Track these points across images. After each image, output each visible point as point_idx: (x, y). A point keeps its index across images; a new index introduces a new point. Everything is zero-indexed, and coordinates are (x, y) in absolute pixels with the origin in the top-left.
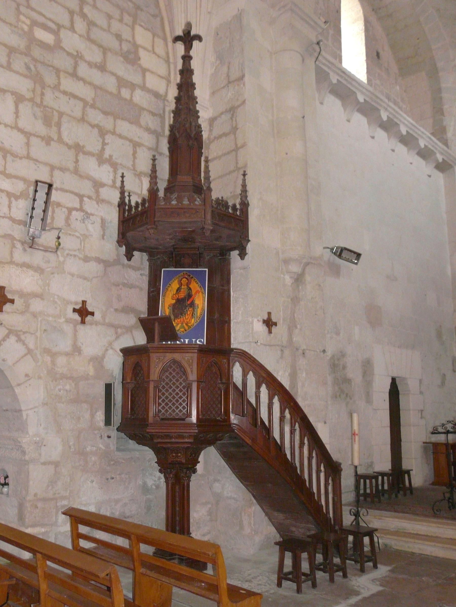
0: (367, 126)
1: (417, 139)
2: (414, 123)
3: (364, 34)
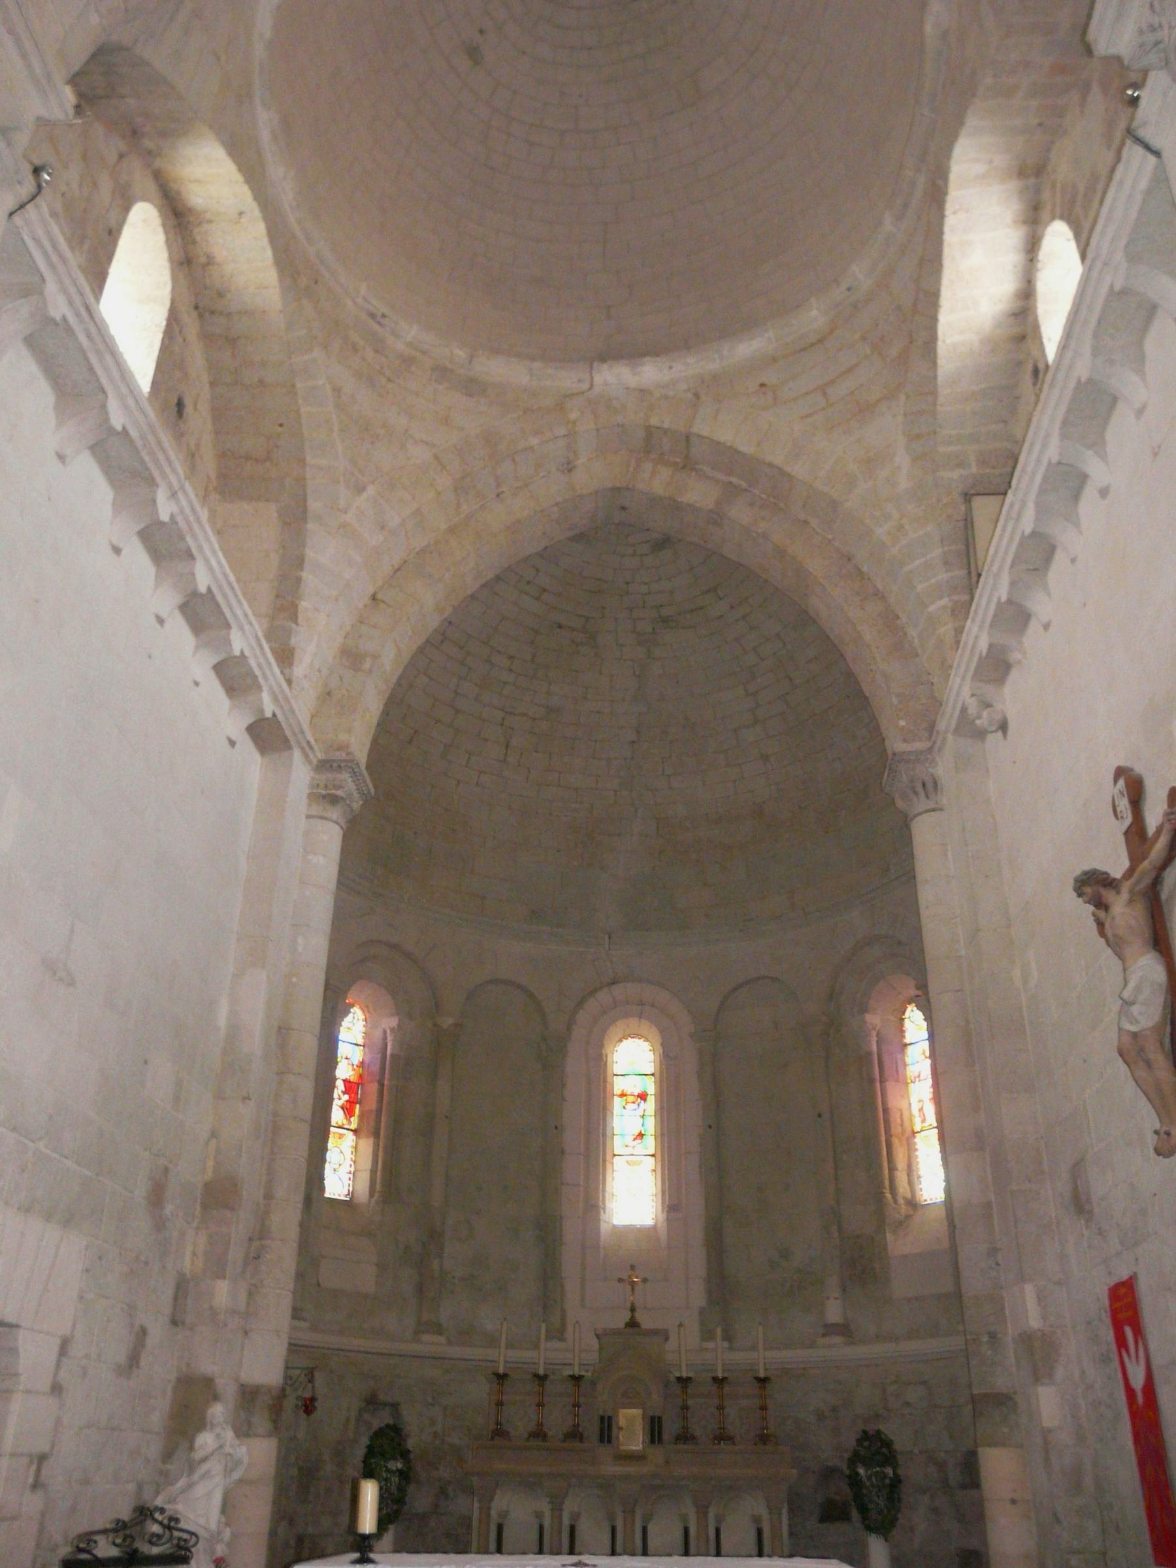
0: (108, 510)
1: (228, 626)
2: (232, 578)
3: (160, 336)
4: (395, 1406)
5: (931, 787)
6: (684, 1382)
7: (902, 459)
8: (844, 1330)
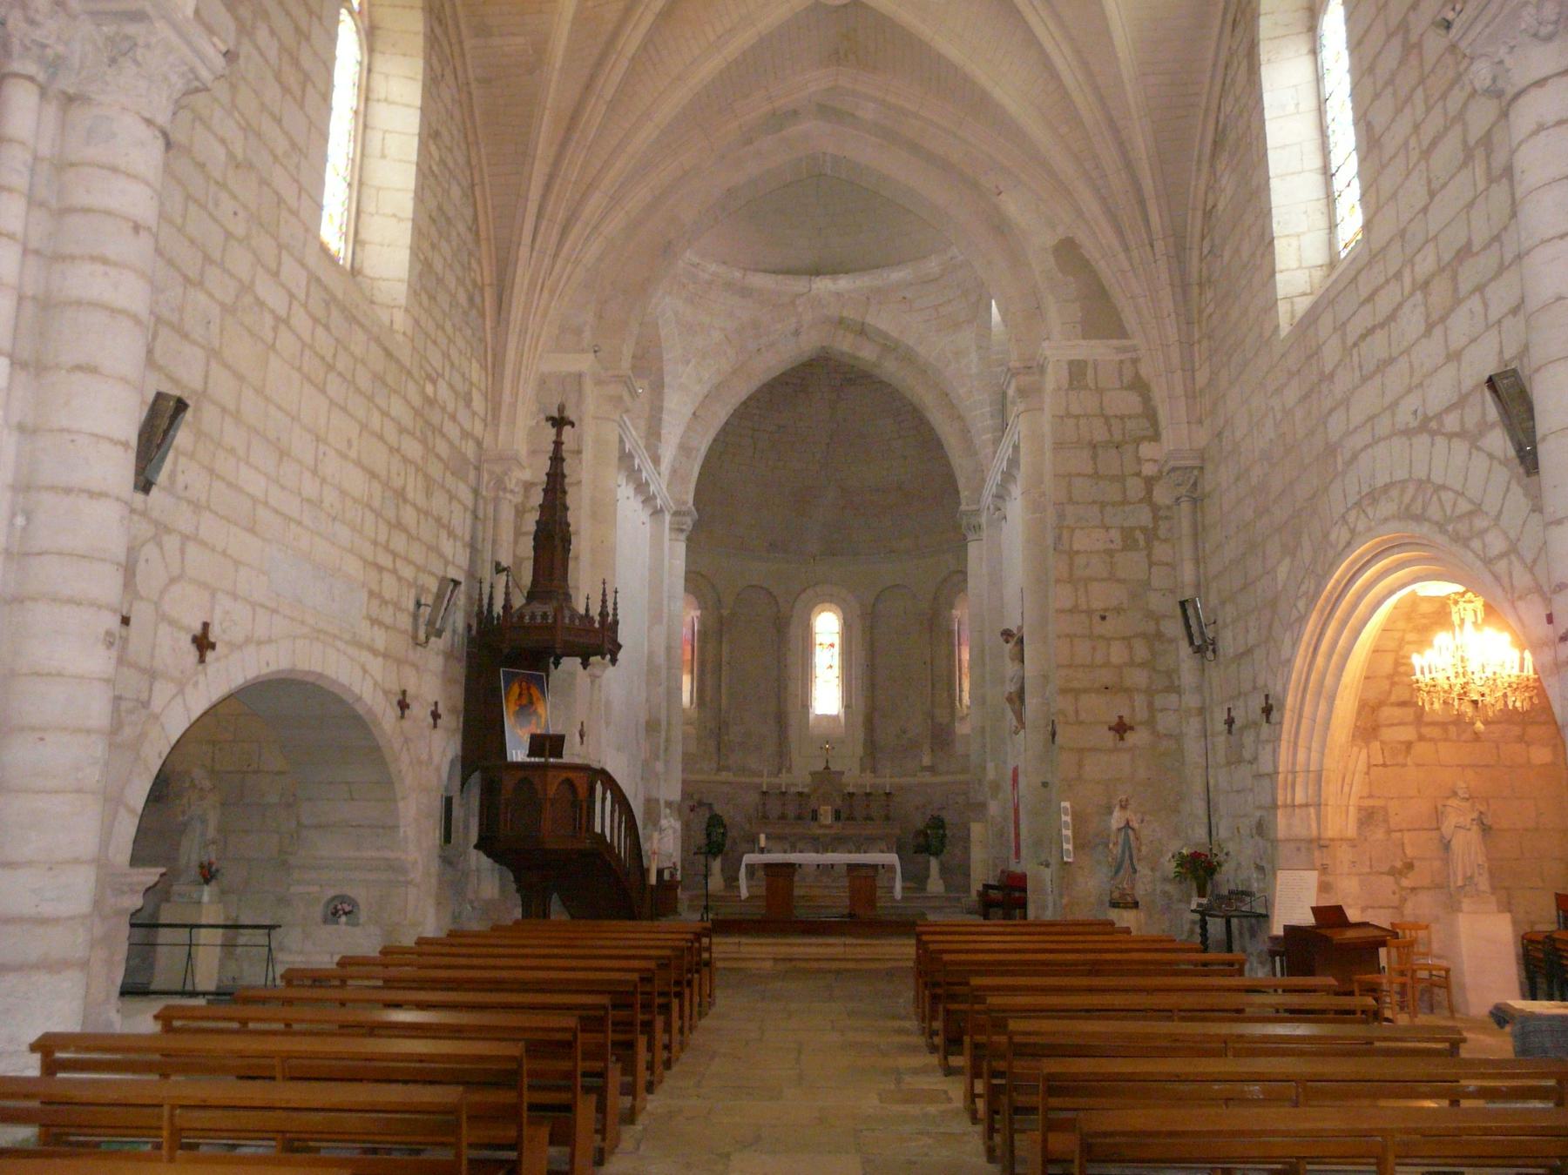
4: (710, 806)
5: (977, 528)
6: (851, 795)
7: (974, 357)
8: (932, 769)
